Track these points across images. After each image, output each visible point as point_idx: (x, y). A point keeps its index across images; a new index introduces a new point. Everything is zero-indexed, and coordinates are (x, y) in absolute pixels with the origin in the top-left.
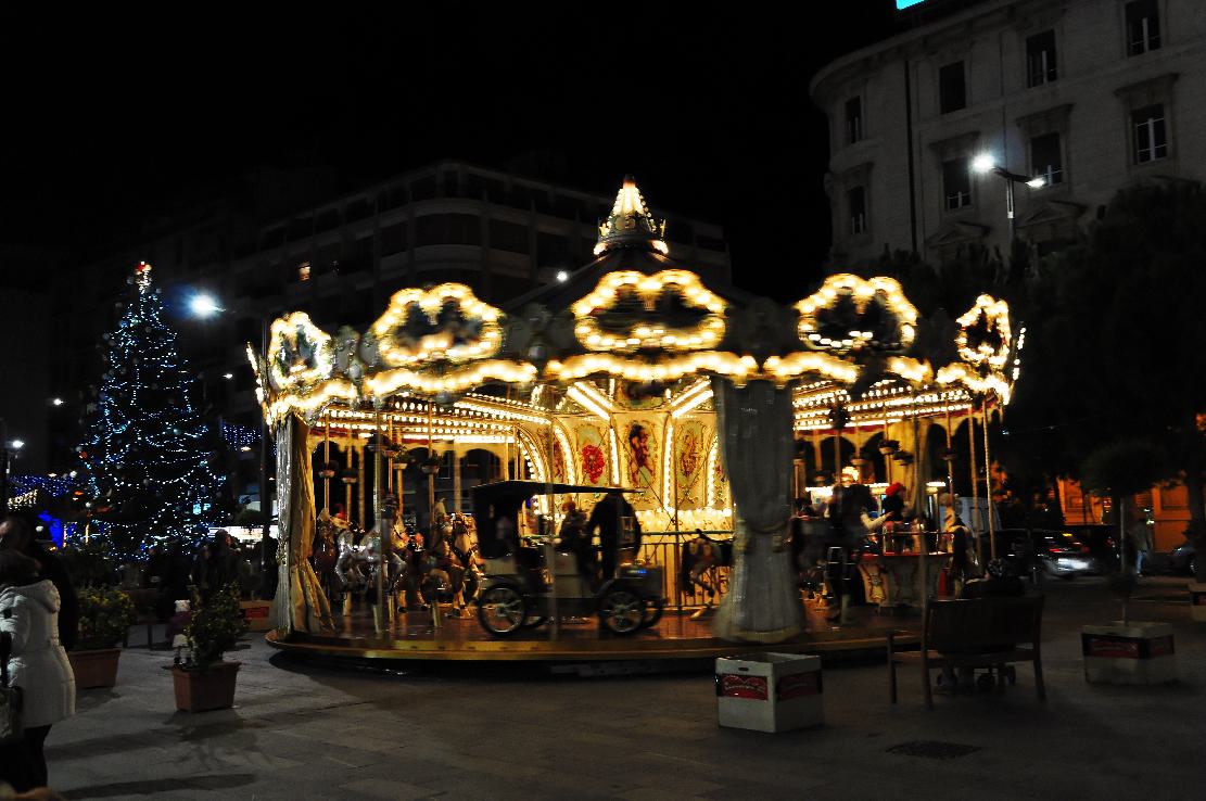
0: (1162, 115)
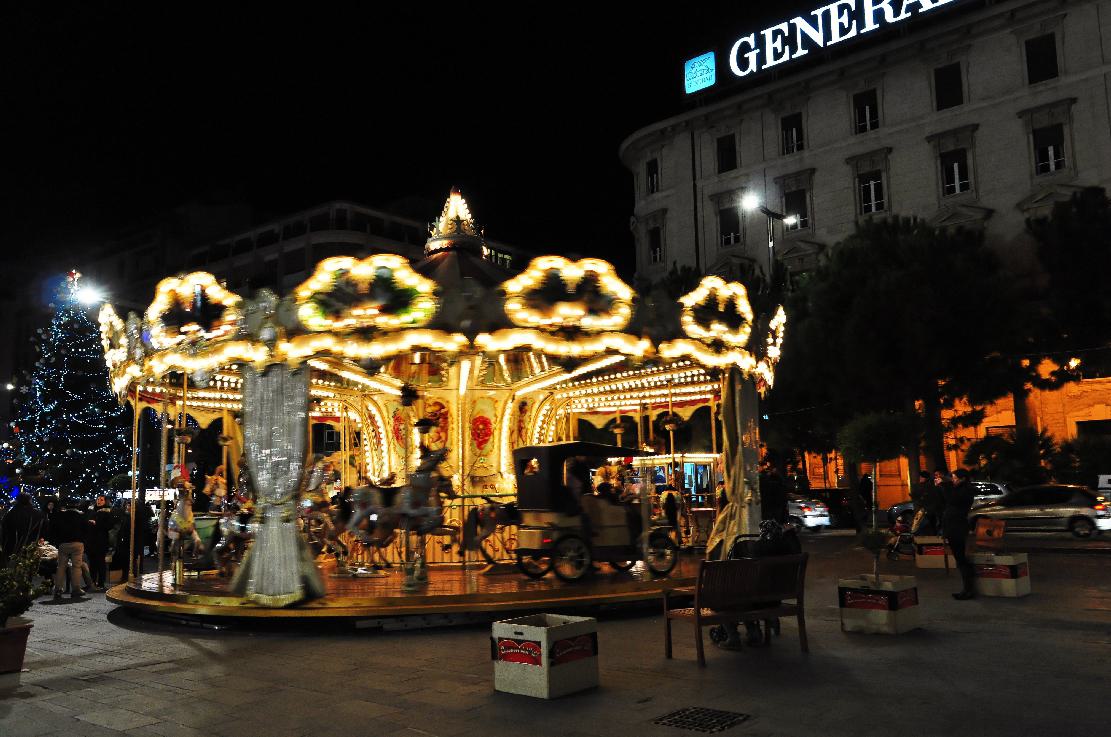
0: (880, 178)
